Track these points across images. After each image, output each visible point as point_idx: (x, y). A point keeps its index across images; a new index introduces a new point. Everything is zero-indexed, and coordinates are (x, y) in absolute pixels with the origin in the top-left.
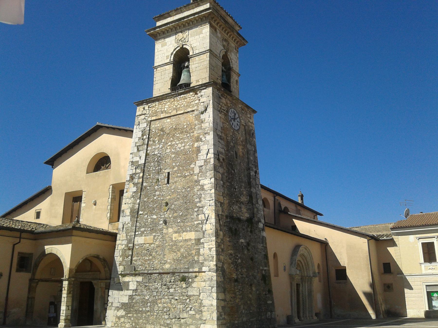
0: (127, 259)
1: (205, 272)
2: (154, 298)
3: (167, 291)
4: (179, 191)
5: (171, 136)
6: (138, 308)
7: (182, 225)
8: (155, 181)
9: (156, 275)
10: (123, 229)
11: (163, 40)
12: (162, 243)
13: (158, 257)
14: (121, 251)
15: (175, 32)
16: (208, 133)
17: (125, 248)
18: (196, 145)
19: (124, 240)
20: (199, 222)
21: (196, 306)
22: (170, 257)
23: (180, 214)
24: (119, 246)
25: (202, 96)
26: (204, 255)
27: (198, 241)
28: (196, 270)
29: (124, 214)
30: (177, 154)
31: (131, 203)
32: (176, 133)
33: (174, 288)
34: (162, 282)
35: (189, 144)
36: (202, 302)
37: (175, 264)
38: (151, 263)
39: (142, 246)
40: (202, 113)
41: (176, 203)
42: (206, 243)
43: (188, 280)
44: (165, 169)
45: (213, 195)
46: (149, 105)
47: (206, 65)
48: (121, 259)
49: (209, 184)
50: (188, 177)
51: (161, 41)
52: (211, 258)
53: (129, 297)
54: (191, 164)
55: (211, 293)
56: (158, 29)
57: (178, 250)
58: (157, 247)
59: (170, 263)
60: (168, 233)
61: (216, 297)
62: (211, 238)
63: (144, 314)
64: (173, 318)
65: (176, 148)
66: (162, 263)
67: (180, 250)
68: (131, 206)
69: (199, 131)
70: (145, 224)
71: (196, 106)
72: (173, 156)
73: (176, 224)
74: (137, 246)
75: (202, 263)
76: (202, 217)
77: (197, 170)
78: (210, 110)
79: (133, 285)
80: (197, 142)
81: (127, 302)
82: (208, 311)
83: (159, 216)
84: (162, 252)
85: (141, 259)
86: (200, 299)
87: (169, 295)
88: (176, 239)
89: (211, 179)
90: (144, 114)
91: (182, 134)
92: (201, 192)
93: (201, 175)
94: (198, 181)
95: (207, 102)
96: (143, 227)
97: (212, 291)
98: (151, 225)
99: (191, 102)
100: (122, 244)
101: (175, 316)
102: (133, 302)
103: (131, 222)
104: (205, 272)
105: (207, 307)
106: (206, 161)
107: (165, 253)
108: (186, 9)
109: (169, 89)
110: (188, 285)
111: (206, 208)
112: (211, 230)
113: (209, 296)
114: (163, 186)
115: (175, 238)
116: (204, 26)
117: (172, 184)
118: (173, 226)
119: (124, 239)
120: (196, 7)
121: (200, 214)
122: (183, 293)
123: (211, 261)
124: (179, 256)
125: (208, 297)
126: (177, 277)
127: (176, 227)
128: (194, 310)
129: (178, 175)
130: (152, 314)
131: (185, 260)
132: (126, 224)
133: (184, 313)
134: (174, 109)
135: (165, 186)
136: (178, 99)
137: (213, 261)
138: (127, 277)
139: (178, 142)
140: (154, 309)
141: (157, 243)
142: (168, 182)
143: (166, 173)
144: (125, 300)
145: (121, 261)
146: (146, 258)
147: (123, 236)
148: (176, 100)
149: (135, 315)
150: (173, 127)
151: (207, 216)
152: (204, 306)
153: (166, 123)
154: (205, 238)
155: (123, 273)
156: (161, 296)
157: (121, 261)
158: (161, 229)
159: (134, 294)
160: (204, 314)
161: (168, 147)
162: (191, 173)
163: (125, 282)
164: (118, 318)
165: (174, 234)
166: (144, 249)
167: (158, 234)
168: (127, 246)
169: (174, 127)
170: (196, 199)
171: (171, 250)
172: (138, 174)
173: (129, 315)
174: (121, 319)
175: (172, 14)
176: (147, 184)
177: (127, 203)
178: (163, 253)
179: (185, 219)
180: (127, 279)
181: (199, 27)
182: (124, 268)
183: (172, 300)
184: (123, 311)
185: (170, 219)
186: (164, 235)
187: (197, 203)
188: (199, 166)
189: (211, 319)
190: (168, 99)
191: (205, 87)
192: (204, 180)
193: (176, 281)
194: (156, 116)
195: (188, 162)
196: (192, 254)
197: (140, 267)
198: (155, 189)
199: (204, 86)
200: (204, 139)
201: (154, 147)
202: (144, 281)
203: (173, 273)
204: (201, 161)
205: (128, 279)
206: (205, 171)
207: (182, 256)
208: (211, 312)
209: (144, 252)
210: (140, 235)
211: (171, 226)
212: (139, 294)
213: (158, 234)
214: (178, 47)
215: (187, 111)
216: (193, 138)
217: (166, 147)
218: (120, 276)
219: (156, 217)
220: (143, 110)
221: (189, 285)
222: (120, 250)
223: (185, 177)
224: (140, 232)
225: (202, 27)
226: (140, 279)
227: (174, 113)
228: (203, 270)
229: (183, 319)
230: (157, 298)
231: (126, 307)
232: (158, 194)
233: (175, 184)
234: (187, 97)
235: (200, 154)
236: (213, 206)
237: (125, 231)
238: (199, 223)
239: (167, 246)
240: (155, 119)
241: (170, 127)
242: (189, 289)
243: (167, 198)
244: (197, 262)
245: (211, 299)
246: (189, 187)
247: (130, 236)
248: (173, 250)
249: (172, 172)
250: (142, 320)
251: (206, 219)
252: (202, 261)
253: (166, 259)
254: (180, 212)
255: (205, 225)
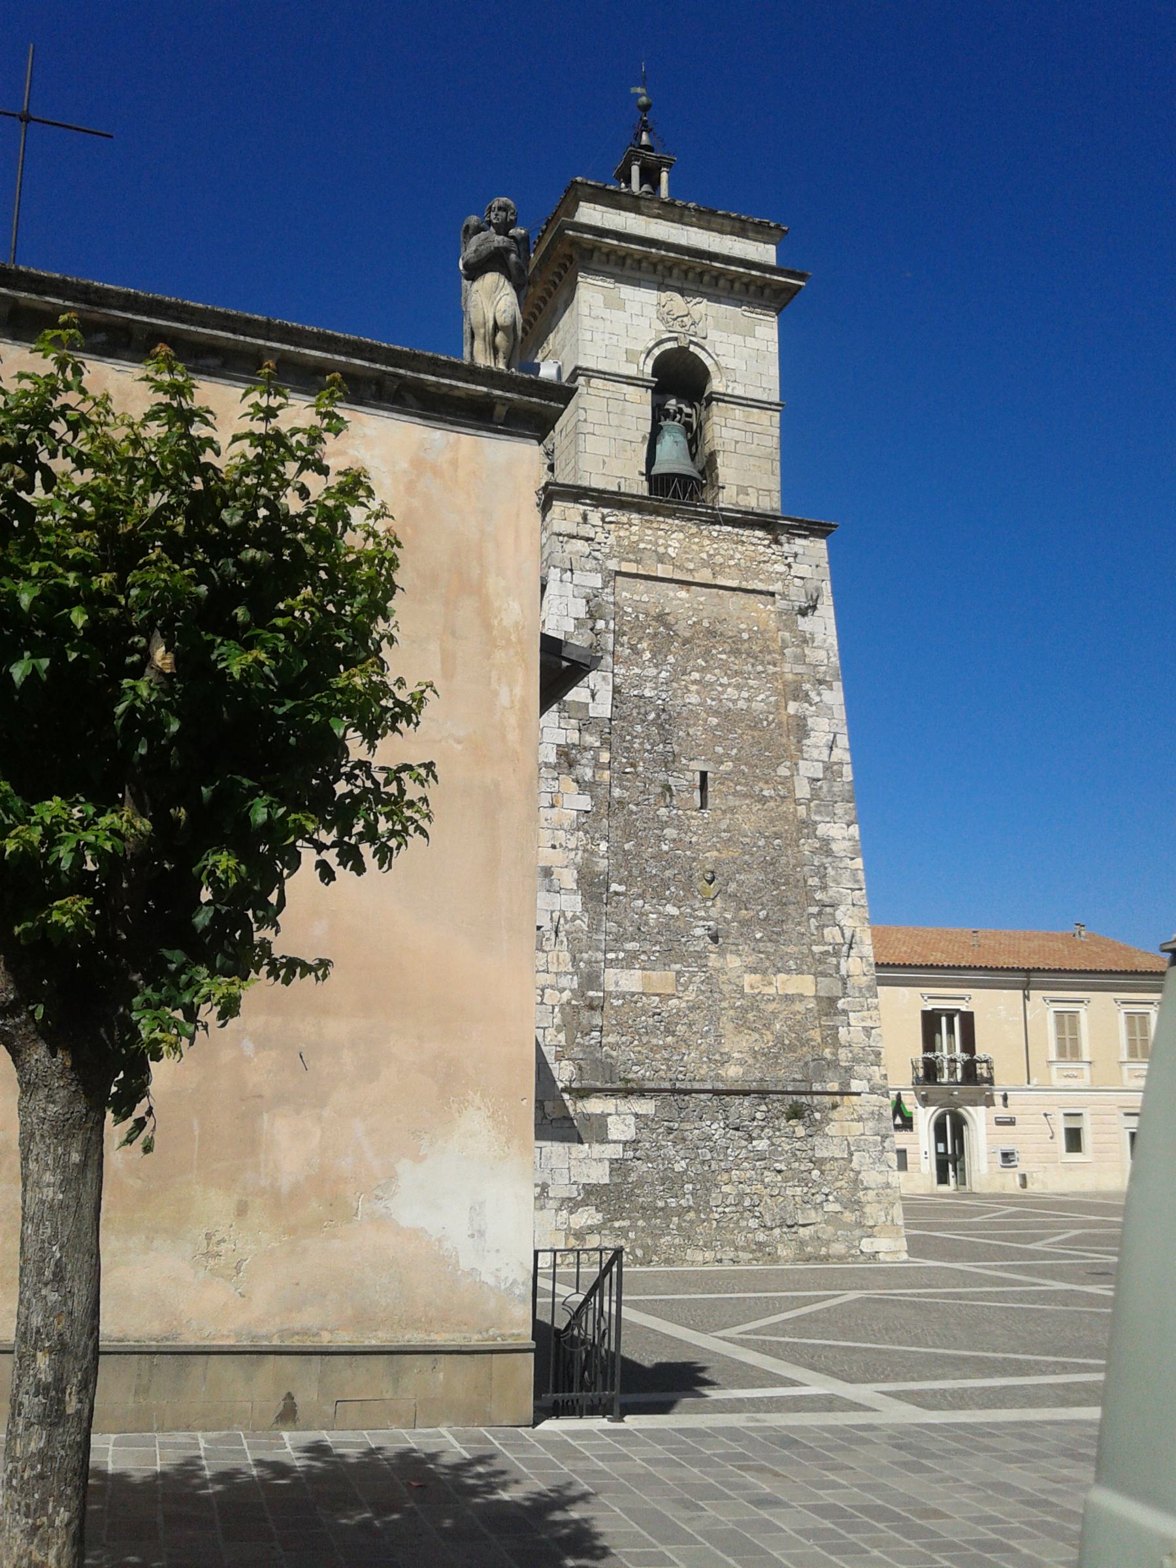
0: (587, 1038)
1: (858, 1094)
2: (706, 1168)
3: (746, 1147)
4: (748, 840)
5: (697, 650)
6: (649, 1200)
7: (772, 951)
8: (659, 790)
9: (703, 1096)
10: (557, 935)
11: (609, 283)
12: (708, 998)
13: (699, 1041)
14: (557, 1009)
15: (660, 279)
16: (827, 682)
17: (574, 1002)
18: (792, 707)
19: (566, 973)
20: (826, 948)
21: (841, 1188)
22: (738, 1045)
23: (762, 914)
24: (547, 991)
25: (796, 555)
26: (850, 1046)
27: (828, 1005)
28: (834, 1086)
29: (551, 881)
30: (729, 718)
31: (577, 848)
32: (714, 647)
33: (769, 1138)
34: (727, 1118)
35: (762, 696)
36: (860, 1177)
37: (758, 1066)
38: (675, 1058)
39: (636, 1003)
40: (803, 612)
41: (742, 877)
42: (854, 1011)
43: (809, 1115)
44: (691, 760)
45: (861, 875)
46: (606, 511)
47: (768, 449)
48: (562, 1037)
49: (844, 838)
50: (772, 804)
51: (600, 283)
52: (872, 1057)
53: (611, 1164)
54: (778, 765)
55: (882, 1152)
56: (611, 239)
57: (764, 1025)
58: (689, 1008)
59: (742, 1062)
60: (726, 970)
61: (896, 1164)
62: (867, 998)
63: (675, 1219)
64: (776, 1226)
65: (722, 697)
66: (716, 1060)
67: (770, 1024)
68: (578, 859)
69: (799, 669)
70: (639, 929)
71: (778, 580)
72: (714, 721)
73: (752, 945)
74: (617, 997)
75: (848, 1070)
76: (831, 933)
77: (803, 790)
78: (827, 608)
79: (622, 1127)
80: (795, 700)
81: (608, 1182)
82: (879, 1202)
83: (688, 910)
84: (711, 1027)
85: (636, 1042)
86: (852, 1170)
87: (756, 1158)
88: (756, 991)
89: (848, 826)
90: (588, 539)
91: (736, 657)
92: (825, 861)
93: (817, 806)
94: (807, 826)
95: (816, 583)
96: (634, 940)
97: (884, 1147)
98: (662, 935)
99: (760, 562)
100: (560, 986)
101: (782, 1218)
102: (630, 1180)
103: (586, 914)
104: (858, 1094)
105: (876, 1191)
106: (828, 767)
107: (720, 1030)
108: (698, 220)
109: (643, 474)
110: (812, 1129)
111: (842, 908)
112: (865, 978)
113: (877, 1160)
114: (689, 812)
115: (752, 987)
116: (761, 317)
117: (719, 812)
118: (740, 948)
119: (566, 969)
120: (732, 234)
121: (828, 926)
122: (798, 1153)
123: (872, 1065)
124: (768, 1042)
125: (874, 1163)
126: (775, 1105)
127: (751, 955)
128: (837, 1200)
129: (738, 788)
130: (703, 1216)
131: (791, 1056)
132: (565, 918)
133: (809, 1212)
134: (705, 564)
135: (694, 813)
136: (715, 534)
137: (879, 1066)
138: (594, 1100)
139: (725, 680)
140: (708, 1202)
141: (690, 995)
142: (703, 805)
143: (693, 771)
144: (600, 1175)
145: (563, 1043)
146: (654, 1041)
147: (560, 961)
148: (705, 533)
149: (641, 1223)
150: (700, 622)
151: (848, 934)
152: (866, 1189)
153: (672, 599)
154: (849, 999)
155: (575, 1085)
156: (727, 1160)
157: (563, 1043)
158: (698, 952)
159: (630, 1154)
160: (868, 1209)
161: (694, 688)
162: (782, 793)
163: (588, 1117)
164: (575, 1235)
165: (746, 976)
166: (644, 1012)
167: (691, 969)
168: (580, 993)
169: (706, 624)
170: (812, 877)
171: (742, 1024)
172: (592, 752)
173: (617, 1224)
174: (587, 1237)
175: (648, 207)
176: (626, 794)
177: (561, 846)
178: (716, 1030)
179: (778, 934)
180: (594, 1106)
181: (743, 308)
182: (580, 1069)
183: (766, 1173)
184: (594, 1212)
185: (728, 924)
186: (712, 972)
187: (814, 889)
188: (808, 778)
189: (889, 1223)
190: (678, 518)
191: (807, 533)
192: (828, 825)
193: (772, 1118)
194: (637, 562)
195: (767, 754)
196: (812, 1040)
197: (634, 1068)
198: (658, 816)
199: (805, 529)
200: (817, 699)
201: (637, 671)
202: (666, 1116)
203: (763, 1094)
204: (815, 763)
205: (601, 1105)
206: (828, 799)
207: (779, 1045)
208: (886, 1205)
209: (646, 1021)
210: (624, 963)
211: (734, 948)
212: (648, 1156)
213: (691, 969)
214: (669, 339)
215: (749, 588)
216: (776, 684)
217: (684, 683)
218: (566, 1096)
219: (678, 913)
220: (580, 519)
221: (815, 1128)
222: (553, 1007)
223: (763, 800)
224: (621, 955)
225: (754, 315)
226: (646, 1107)
227: (704, 576)
228: (853, 1089)
229: (804, 1226)
230: (714, 1166)
231: (604, 1198)
232: (675, 836)
233: (729, 816)
234: (744, 538)
235: (805, 742)
236: (863, 906)
237: (565, 943)
238: (827, 953)
239: (725, 1009)
240: (635, 571)
241: (690, 618)
242: (817, 1140)
243: (708, 855)
244: (834, 1064)
245: (884, 1168)
246: (777, 836)
247: (589, 962)
248: (748, 1024)
249: (715, 774)
250: (669, 1238)
251: (848, 941)
252: (847, 1064)
253: (727, 1050)
254: (760, 907)
255: (846, 961)
